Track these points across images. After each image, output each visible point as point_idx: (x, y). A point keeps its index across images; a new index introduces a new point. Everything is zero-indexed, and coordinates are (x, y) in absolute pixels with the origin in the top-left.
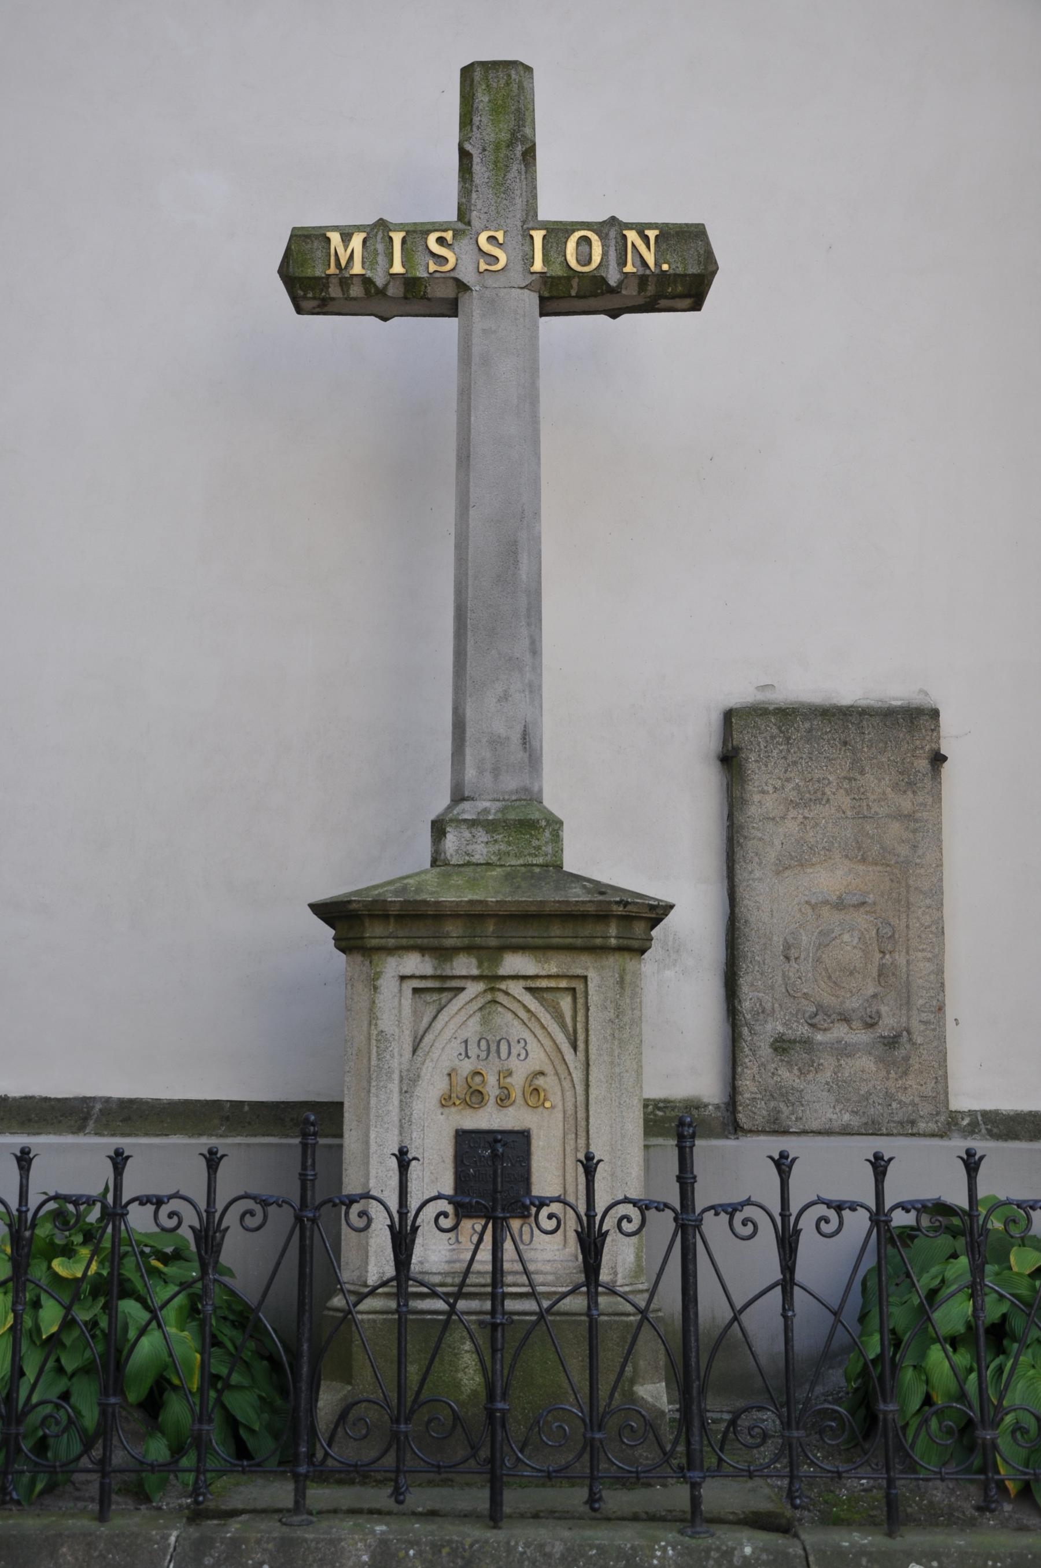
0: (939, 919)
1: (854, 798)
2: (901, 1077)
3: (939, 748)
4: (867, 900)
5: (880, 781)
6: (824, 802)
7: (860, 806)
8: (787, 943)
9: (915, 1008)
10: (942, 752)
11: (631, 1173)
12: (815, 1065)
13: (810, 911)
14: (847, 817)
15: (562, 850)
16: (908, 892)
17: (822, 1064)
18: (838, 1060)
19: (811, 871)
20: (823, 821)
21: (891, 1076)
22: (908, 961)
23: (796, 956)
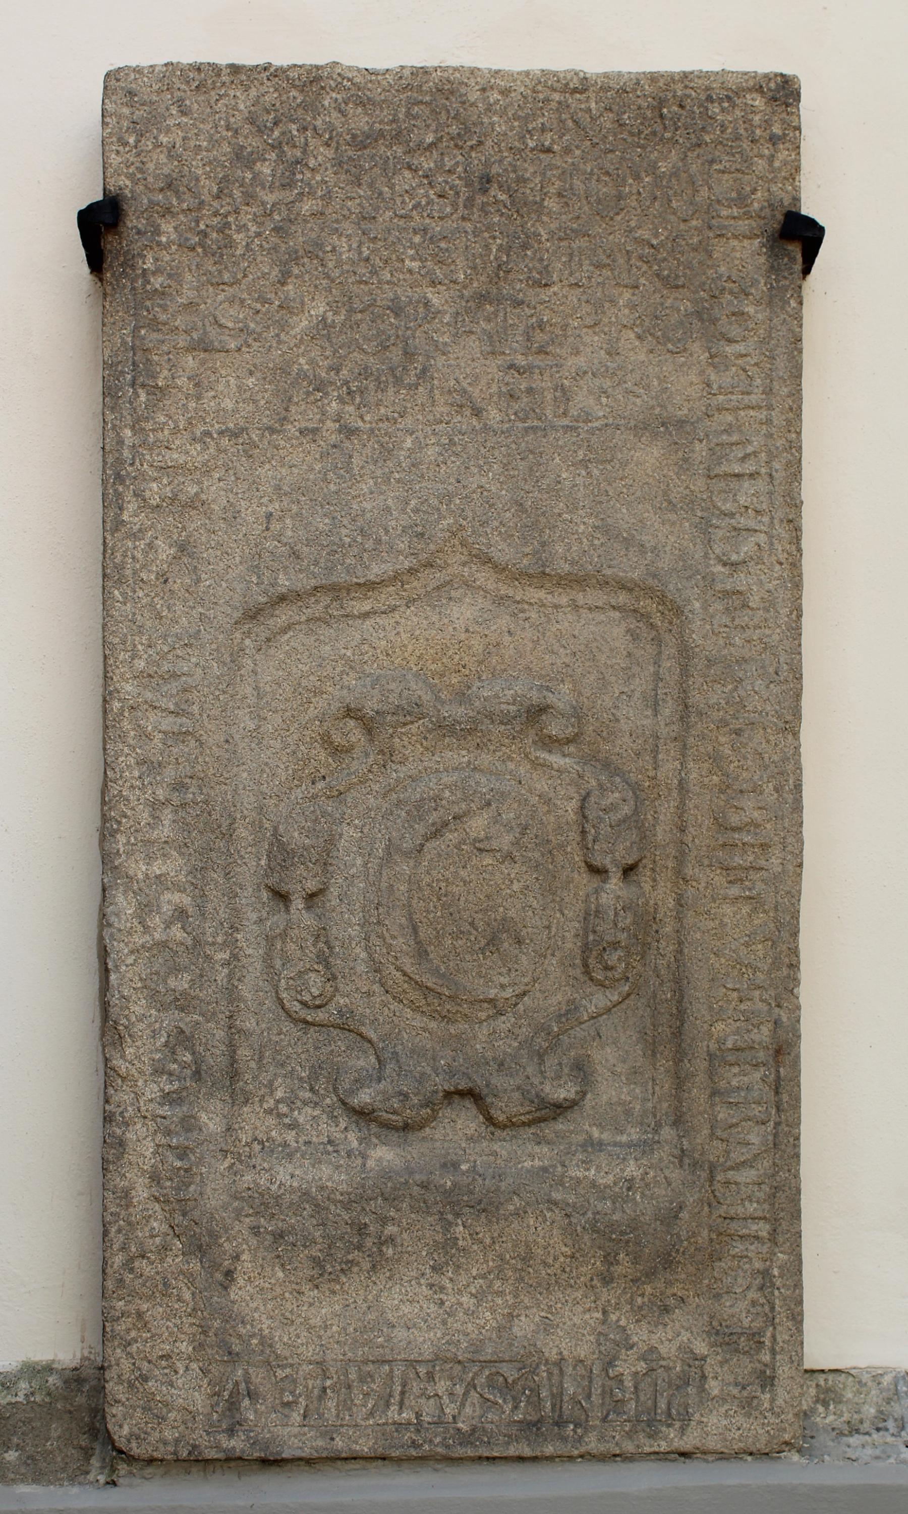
0: (785, 760)
1: (511, 366)
2: (651, 1274)
3: (796, 200)
4: (551, 699)
5: (598, 307)
6: (411, 379)
7: (530, 391)
8: (282, 846)
9: (188, 991)
10: (806, 210)
11: (764, 1342)
12: (369, 1242)
13: (357, 735)
14: (486, 428)
15: (799, 912)
16: (685, 672)
17: (391, 1239)
18: (448, 1226)
19: (367, 607)
20: (409, 443)
21: (618, 1270)
22: (680, 902)
23: (312, 885)
